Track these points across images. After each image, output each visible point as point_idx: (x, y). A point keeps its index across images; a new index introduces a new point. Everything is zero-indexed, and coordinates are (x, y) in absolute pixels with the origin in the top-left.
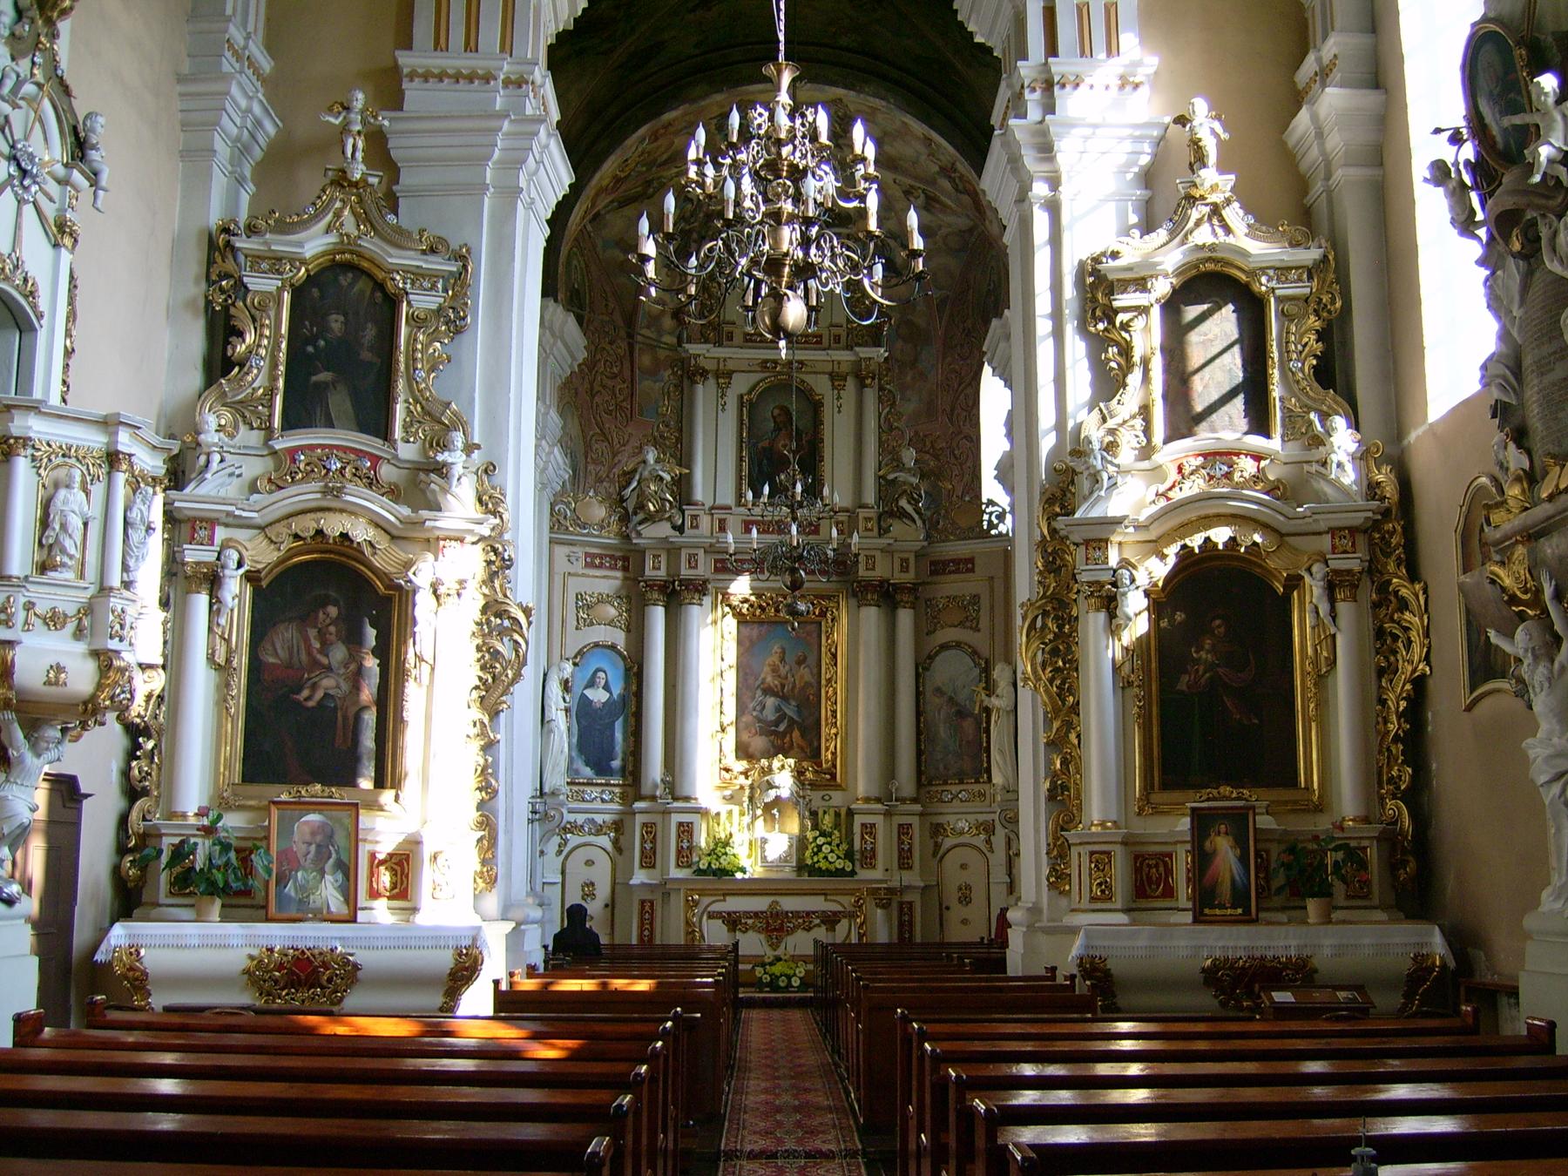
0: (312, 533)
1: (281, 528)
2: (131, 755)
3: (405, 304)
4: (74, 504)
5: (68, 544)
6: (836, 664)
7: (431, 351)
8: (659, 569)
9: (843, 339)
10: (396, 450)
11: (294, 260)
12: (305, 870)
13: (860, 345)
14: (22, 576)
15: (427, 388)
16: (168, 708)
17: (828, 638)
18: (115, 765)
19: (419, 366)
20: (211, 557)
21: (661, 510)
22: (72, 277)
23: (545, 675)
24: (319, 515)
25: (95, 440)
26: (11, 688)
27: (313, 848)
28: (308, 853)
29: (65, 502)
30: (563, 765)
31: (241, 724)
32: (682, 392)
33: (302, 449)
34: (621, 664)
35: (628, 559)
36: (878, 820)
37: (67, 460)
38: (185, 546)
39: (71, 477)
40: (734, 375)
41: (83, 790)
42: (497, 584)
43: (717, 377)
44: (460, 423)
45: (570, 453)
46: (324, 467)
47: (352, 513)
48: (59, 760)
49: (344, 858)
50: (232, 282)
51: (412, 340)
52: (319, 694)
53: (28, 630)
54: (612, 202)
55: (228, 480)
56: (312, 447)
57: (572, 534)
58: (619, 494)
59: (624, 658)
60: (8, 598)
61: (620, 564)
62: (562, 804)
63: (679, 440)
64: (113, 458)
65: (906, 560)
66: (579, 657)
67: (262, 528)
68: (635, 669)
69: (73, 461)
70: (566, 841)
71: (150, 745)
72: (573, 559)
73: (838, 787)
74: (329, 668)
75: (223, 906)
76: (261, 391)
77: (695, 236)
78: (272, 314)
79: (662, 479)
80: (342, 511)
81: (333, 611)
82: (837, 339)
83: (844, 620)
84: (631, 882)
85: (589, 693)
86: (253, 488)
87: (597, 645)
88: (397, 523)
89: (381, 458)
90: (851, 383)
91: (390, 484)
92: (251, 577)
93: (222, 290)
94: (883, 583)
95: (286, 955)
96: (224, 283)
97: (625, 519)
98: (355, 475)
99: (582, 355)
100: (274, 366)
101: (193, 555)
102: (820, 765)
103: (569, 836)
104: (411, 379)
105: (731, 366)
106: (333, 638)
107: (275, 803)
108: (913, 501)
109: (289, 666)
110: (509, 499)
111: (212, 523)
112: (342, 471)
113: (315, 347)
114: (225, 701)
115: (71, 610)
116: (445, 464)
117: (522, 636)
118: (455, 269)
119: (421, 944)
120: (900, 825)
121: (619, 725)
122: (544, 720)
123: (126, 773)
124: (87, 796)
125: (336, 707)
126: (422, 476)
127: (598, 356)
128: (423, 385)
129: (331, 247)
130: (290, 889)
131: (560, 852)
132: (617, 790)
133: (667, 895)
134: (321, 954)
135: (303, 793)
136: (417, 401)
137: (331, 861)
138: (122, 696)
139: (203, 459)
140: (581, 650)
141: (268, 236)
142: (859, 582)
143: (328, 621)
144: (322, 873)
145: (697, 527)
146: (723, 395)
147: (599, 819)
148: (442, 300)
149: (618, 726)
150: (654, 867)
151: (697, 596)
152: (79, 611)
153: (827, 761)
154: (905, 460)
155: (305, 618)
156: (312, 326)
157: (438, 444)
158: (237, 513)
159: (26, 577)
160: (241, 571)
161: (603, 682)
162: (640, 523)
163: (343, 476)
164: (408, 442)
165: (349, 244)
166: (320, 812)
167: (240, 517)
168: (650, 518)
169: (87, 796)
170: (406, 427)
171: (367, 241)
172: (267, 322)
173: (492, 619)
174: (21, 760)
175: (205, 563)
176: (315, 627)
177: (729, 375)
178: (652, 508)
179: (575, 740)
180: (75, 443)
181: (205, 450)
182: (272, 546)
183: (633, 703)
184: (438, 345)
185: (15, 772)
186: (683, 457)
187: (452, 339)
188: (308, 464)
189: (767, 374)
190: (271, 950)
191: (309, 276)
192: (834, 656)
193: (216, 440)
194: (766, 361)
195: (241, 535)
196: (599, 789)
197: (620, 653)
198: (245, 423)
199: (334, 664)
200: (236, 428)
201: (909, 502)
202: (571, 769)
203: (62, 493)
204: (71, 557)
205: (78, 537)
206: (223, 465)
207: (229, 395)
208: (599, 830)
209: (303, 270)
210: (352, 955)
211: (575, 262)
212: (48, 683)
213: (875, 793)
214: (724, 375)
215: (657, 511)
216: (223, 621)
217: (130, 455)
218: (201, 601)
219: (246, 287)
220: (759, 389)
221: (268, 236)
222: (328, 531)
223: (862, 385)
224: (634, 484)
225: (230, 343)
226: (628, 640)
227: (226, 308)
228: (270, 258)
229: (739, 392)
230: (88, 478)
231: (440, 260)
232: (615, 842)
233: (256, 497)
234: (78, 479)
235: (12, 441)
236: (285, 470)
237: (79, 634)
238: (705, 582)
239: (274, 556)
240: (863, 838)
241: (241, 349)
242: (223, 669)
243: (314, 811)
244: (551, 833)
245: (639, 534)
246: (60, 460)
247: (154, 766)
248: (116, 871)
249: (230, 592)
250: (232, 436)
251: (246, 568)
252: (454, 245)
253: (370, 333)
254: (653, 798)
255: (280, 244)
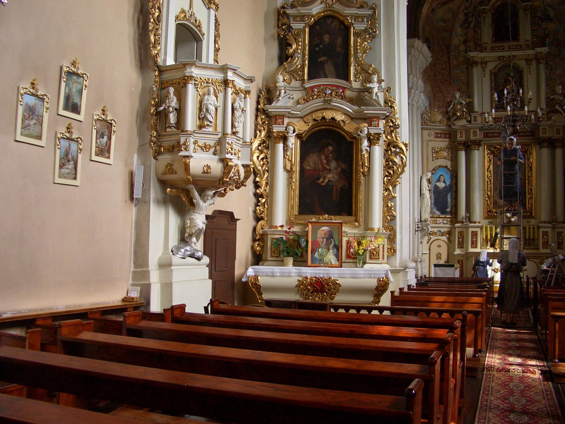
0: (320, 118)
1: (309, 118)
2: (257, 205)
3: (352, 28)
4: (211, 101)
5: (209, 117)
6: (531, 171)
7: (363, 45)
8: (462, 137)
9: (530, 46)
10: (351, 84)
11: (309, 16)
12: (322, 248)
13: (536, 47)
14: (192, 131)
15: (363, 60)
16: (270, 187)
17: (528, 161)
18: (251, 209)
19: (359, 51)
20: (283, 129)
21: (462, 115)
22: (216, 20)
23: (421, 177)
24: (323, 111)
25: (219, 76)
26: (189, 175)
27: (325, 240)
28: (323, 242)
29: (208, 100)
30: (429, 210)
31: (297, 192)
32: (468, 71)
33: (315, 86)
34: (449, 173)
35: (450, 134)
36: (549, 230)
37: (208, 84)
38: (273, 126)
39: (209, 91)
40: (488, 63)
41: (236, 217)
42: (393, 135)
43: (482, 64)
44: (376, 72)
45: (428, 98)
46: (324, 93)
47: (335, 110)
48: (214, 204)
49: (337, 243)
50: (286, 26)
51: (356, 42)
52: (326, 181)
53: (195, 152)
54: (438, 4)
55: (288, 100)
56: (319, 86)
57: (429, 125)
58: (446, 110)
59: (450, 171)
60: (186, 139)
61: (448, 136)
62: (428, 225)
63: (468, 89)
64: (226, 83)
65: (559, 129)
66: (434, 171)
67: (302, 118)
68: (455, 175)
69: (211, 85)
70: (430, 238)
71: (264, 200)
72: (430, 135)
73: (534, 218)
74: (330, 170)
75: (294, 261)
76: (299, 66)
77: (470, 15)
78: (302, 37)
79: (462, 103)
80: (331, 109)
81: (331, 148)
82: (528, 46)
83: (534, 154)
84: (455, 253)
85: (438, 184)
86: (298, 103)
87: (440, 166)
88: (353, 113)
89: (345, 88)
90: (534, 62)
91: (350, 98)
92: (299, 136)
93: (283, 30)
94: (550, 138)
95: (312, 280)
96: (283, 27)
97: (449, 119)
98: (336, 95)
99: (430, 60)
100: (304, 56)
101: (276, 129)
102: (526, 209)
103: (431, 236)
104: (356, 57)
105: (486, 60)
106: (331, 159)
107: (310, 222)
108: (561, 106)
109: (315, 170)
110: (397, 102)
111: (283, 117)
112: (331, 94)
113: (319, 48)
114: (291, 183)
115: (212, 144)
116: (371, 88)
117: (404, 155)
118: (371, 13)
119: (366, 276)
120: (558, 232)
121: (449, 195)
122: (421, 194)
123: (255, 212)
124: (238, 220)
125: (333, 186)
126: (362, 94)
127: (437, 62)
128: (361, 59)
129: (323, 9)
130: (316, 255)
131: (428, 242)
132: (449, 220)
133: (467, 258)
134: (326, 280)
135: (321, 218)
136: (359, 65)
137: (332, 245)
138: (235, 177)
139: (278, 92)
140: (434, 168)
141: (299, 8)
142: (540, 139)
143: (329, 152)
144: (329, 249)
145: (476, 121)
146: (484, 71)
147: (442, 230)
148: (367, 25)
149: (449, 196)
150: (463, 248)
151: (477, 147)
152: (215, 144)
153: (529, 208)
154: (557, 91)
155: (321, 150)
156: (317, 40)
157: (368, 81)
158: (292, 112)
159: (194, 131)
160: (295, 134)
161: (443, 180)
162: (455, 120)
163: (332, 96)
164: (356, 81)
165: (329, 7)
166: (327, 226)
167: (293, 114)
168: (459, 118)
169: (238, 220)
170: (355, 76)
171: (336, 5)
172: (300, 40)
173: (392, 149)
174: (199, 204)
175: (281, 132)
176: (323, 155)
177: (486, 63)
178: (459, 114)
179: (433, 201)
180: (211, 78)
181: (279, 89)
182: (306, 124)
183: (454, 187)
184: (366, 43)
185: (197, 208)
186: (470, 95)
187: (371, 40)
188: (318, 92)
189: (500, 62)
190: (307, 278)
191: (315, 21)
192: (531, 168)
193: (283, 85)
194: (500, 57)
195: (294, 121)
196: (442, 219)
197: (448, 169)
198: (294, 78)
199: (332, 169)
200: (291, 81)
201: (559, 107)
202: (432, 212)
203: (206, 97)
204: (211, 122)
205: (213, 113)
206: (286, 94)
207: (288, 69)
208: (443, 234)
209: (313, 19)
210: (337, 280)
211: (426, 28)
212: (204, 172)
213: (547, 220)
214: (484, 63)
215: (460, 116)
216: (289, 153)
217: (233, 81)
218: (281, 146)
219: (292, 28)
220: (498, 67)
221: (299, 8)
222: (326, 117)
223: (538, 62)
224: (452, 106)
225: (287, 49)
226: (451, 164)
227: (285, 36)
228: (300, 16)
229: (491, 69)
230: (217, 91)
231: (365, 10)
232: (449, 239)
233: (299, 106)
234: (212, 91)
235: (186, 78)
236: (309, 94)
237: (215, 154)
238: (481, 141)
239: (306, 128)
240: (543, 237)
241: (291, 51)
242: (290, 172)
243: (325, 226)
244: (425, 235)
245: (454, 125)
246: (205, 84)
247: (265, 209)
248: (252, 247)
249: (291, 142)
250: (289, 84)
251: (296, 133)
252: (370, 4)
253: (340, 40)
254: (462, 222)
255: (303, 10)
